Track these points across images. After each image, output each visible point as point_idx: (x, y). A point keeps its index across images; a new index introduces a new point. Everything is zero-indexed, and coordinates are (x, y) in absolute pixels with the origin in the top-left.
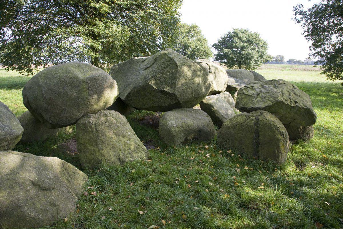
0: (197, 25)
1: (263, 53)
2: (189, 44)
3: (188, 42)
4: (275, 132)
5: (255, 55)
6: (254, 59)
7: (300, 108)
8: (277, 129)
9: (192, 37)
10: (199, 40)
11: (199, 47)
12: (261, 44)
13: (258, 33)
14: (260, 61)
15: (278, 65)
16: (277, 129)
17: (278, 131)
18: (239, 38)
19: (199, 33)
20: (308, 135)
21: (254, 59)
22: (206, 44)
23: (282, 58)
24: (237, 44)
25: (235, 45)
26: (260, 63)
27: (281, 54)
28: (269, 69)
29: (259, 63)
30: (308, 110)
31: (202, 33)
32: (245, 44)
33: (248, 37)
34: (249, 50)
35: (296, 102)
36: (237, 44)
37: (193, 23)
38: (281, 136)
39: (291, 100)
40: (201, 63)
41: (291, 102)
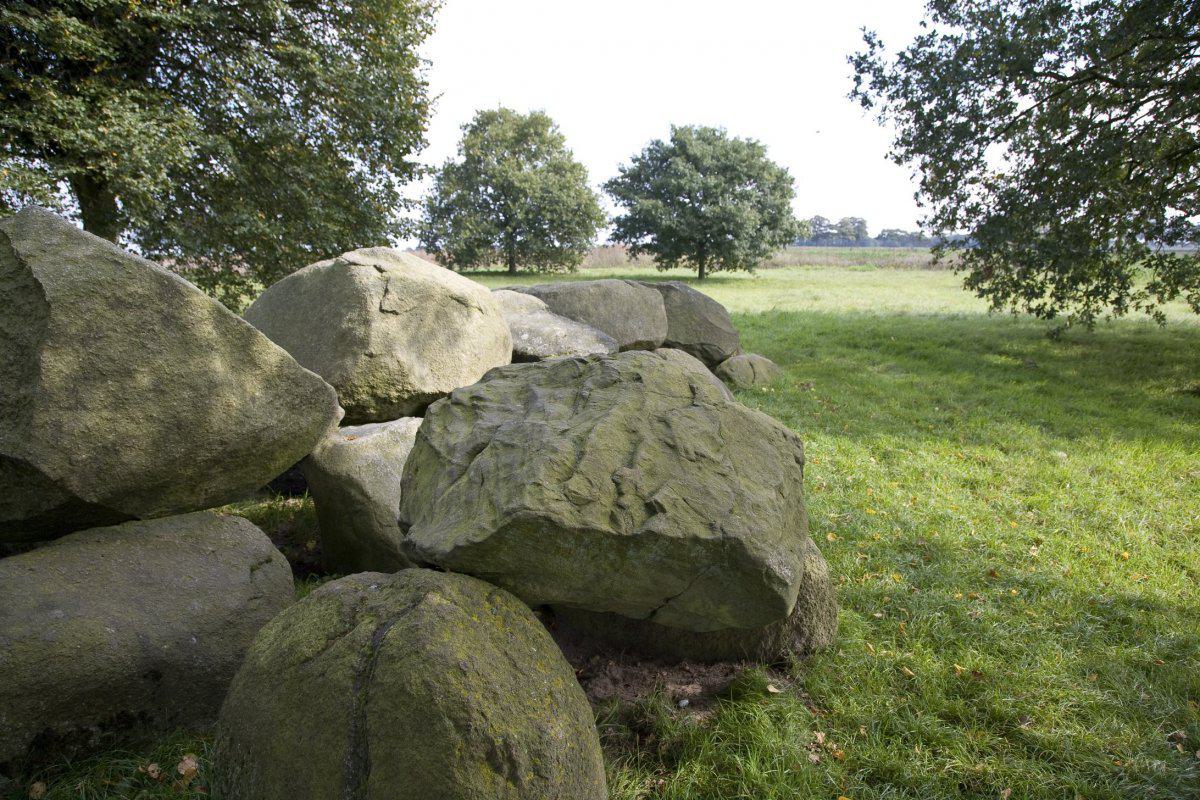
0: (549, 114)
1: (779, 209)
2: (517, 184)
3: (515, 177)
4: (449, 748)
5: (750, 216)
6: (747, 234)
7: (678, 549)
8: (464, 728)
9: (533, 156)
10: (558, 169)
11: (556, 192)
12: (769, 179)
13: (758, 141)
14: (768, 238)
15: (846, 250)
16: (467, 728)
17: (467, 741)
18: (694, 161)
19: (556, 143)
20: (801, 633)
21: (747, 234)
22: (584, 183)
23: (861, 225)
24: (682, 182)
25: (679, 183)
26: (768, 247)
27: (858, 215)
28: (806, 266)
29: (764, 246)
30: (733, 548)
31: (567, 146)
32: (712, 181)
33: (723, 155)
34: (730, 204)
35: (653, 509)
36: (682, 182)
37: (537, 109)
38: (498, 769)
39: (620, 494)
40: (355, 264)
41: (617, 511)
